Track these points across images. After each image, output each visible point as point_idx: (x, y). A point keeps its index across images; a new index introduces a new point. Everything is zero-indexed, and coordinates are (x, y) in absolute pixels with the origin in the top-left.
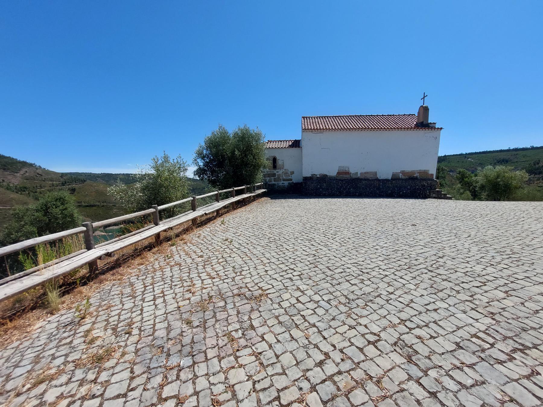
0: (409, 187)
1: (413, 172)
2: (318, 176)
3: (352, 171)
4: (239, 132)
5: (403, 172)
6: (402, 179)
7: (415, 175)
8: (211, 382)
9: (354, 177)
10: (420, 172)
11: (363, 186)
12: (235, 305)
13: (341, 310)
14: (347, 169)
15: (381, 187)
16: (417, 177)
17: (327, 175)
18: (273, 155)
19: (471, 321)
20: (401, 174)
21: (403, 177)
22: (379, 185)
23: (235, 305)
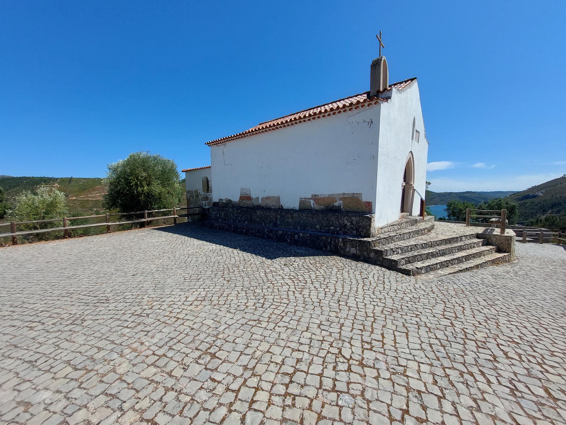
0: (318, 226)
1: (332, 198)
2: (224, 201)
3: (253, 196)
4: (169, 166)
5: (315, 198)
6: (317, 211)
7: (336, 204)
8: (298, 373)
9: (255, 203)
10: (344, 198)
11: (258, 219)
12: (295, 312)
13: (437, 402)
14: (248, 193)
15: (279, 222)
16: (339, 207)
17: (231, 201)
18: (205, 176)
19: (98, 317)
20: (312, 202)
21: (317, 207)
22: (276, 219)
23: (295, 312)
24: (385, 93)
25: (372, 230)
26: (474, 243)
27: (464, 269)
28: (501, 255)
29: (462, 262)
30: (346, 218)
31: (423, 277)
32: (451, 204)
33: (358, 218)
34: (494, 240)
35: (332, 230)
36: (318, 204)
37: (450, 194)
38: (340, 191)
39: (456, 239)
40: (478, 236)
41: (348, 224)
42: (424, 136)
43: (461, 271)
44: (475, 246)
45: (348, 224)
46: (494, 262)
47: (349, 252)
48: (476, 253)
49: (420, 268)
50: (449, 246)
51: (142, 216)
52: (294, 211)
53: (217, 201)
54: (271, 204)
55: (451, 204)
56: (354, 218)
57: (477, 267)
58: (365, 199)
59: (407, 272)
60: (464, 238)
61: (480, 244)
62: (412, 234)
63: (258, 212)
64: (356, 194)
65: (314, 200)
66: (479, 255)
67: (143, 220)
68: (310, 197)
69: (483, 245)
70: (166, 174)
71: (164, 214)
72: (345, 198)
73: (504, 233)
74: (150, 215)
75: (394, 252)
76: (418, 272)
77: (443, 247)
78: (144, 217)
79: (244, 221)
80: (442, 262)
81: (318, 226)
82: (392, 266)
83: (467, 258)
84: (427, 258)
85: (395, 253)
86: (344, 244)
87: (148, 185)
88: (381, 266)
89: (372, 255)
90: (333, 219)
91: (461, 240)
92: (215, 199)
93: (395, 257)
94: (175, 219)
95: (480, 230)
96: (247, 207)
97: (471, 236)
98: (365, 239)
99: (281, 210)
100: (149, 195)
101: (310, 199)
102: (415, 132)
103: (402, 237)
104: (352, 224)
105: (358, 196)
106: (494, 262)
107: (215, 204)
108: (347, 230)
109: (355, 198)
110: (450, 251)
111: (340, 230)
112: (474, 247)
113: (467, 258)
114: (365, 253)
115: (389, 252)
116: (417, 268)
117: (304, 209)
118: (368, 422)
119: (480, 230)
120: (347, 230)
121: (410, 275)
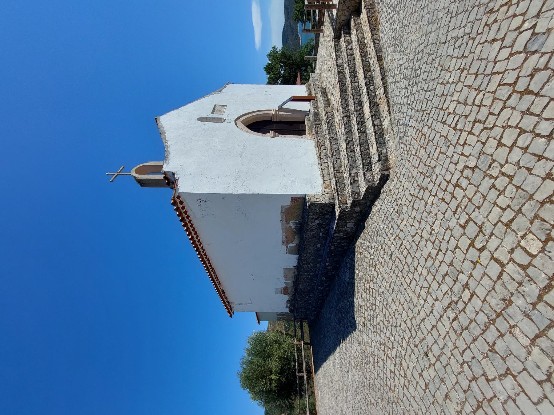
1: (286, 231)
5: (285, 243)
7: (293, 226)
11: (308, 288)
20: (290, 245)
24: (169, 177)
25: (325, 200)
26: (347, 49)
27: (383, 84)
28: (364, 11)
29: (372, 78)
30: (309, 223)
31: (393, 157)
32: (297, 18)
33: (311, 214)
34: (343, 18)
35: (324, 248)
36: (293, 241)
37: (286, 7)
38: (280, 224)
39: (341, 74)
40: (337, 37)
41: (317, 222)
42: (220, 94)
43: (386, 91)
44: (350, 47)
45: (317, 222)
46: (374, 28)
47: (351, 228)
48: (361, 52)
49: (379, 156)
50: (349, 90)
51: (301, 378)
52: (299, 260)
53: (288, 309)
54: (292, 274)
55: (297, 18)
56: (311, 217)
57: (380, 59)
58: (288, 203)
59: (384, 179)
60: (340, 61)
61: (348, 38)
62: (332, 135)
63: (301, 287)
64: (282, 210)
65: (288, 243)
66: (362, 45)
67: (305, 378)
68: (285, 247)
69: (350, 34)
70: (261, 347)
71: (300, 356)
72: (286, 220)
73: (335, 5)
74: (301, 371)
75: (355, 181)
76: (384, 159)
77: (354, 122)
78: (303, 377)
79: (309, 297)
80: (372, 116)
81: (319, 246)
82: (374, 193)
83: (367, 68)
84: (365, 132)
85: (356, 178)
86: (342, 232)
87: (271, 374)
88: (372, 202)
89: (357, 209)
90: (310, 234)
91: (342, 65)
92: (287, 310)
93: (363, 188)
94: (305, 343)
95: (328, 30)
96: (295, 290)
97: (337, 48)
98: (337, 215)
99: (299, 268)
100: (282, 372)
101: (287, 247)
102: (215, 116)
103: (336, 152)
104: (317, 219)
105: (284, 209)
106: (374, 28)
107: (291, 311)
108: (324, 222)
109: (287, 213)
110: (357, 90)
111: (324, 228)
112: (351, 49)
113: (367, 68)
114: (354, 215)
115: (355, 189)
116: (379, 161)
117: (299, 250)
118: (552, 99)
119: (328, 30)
120: (324, 222)
121: (388, 175)
